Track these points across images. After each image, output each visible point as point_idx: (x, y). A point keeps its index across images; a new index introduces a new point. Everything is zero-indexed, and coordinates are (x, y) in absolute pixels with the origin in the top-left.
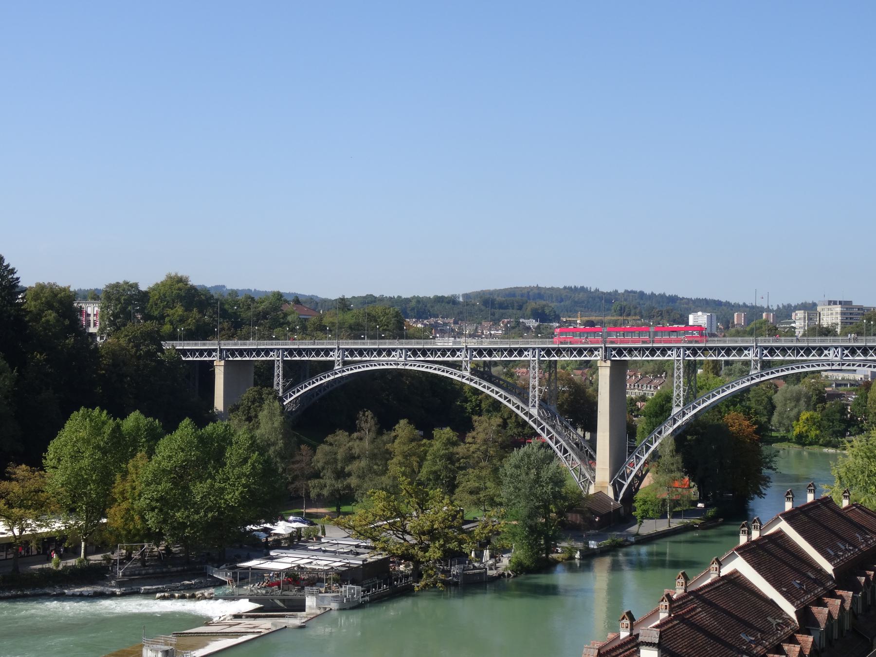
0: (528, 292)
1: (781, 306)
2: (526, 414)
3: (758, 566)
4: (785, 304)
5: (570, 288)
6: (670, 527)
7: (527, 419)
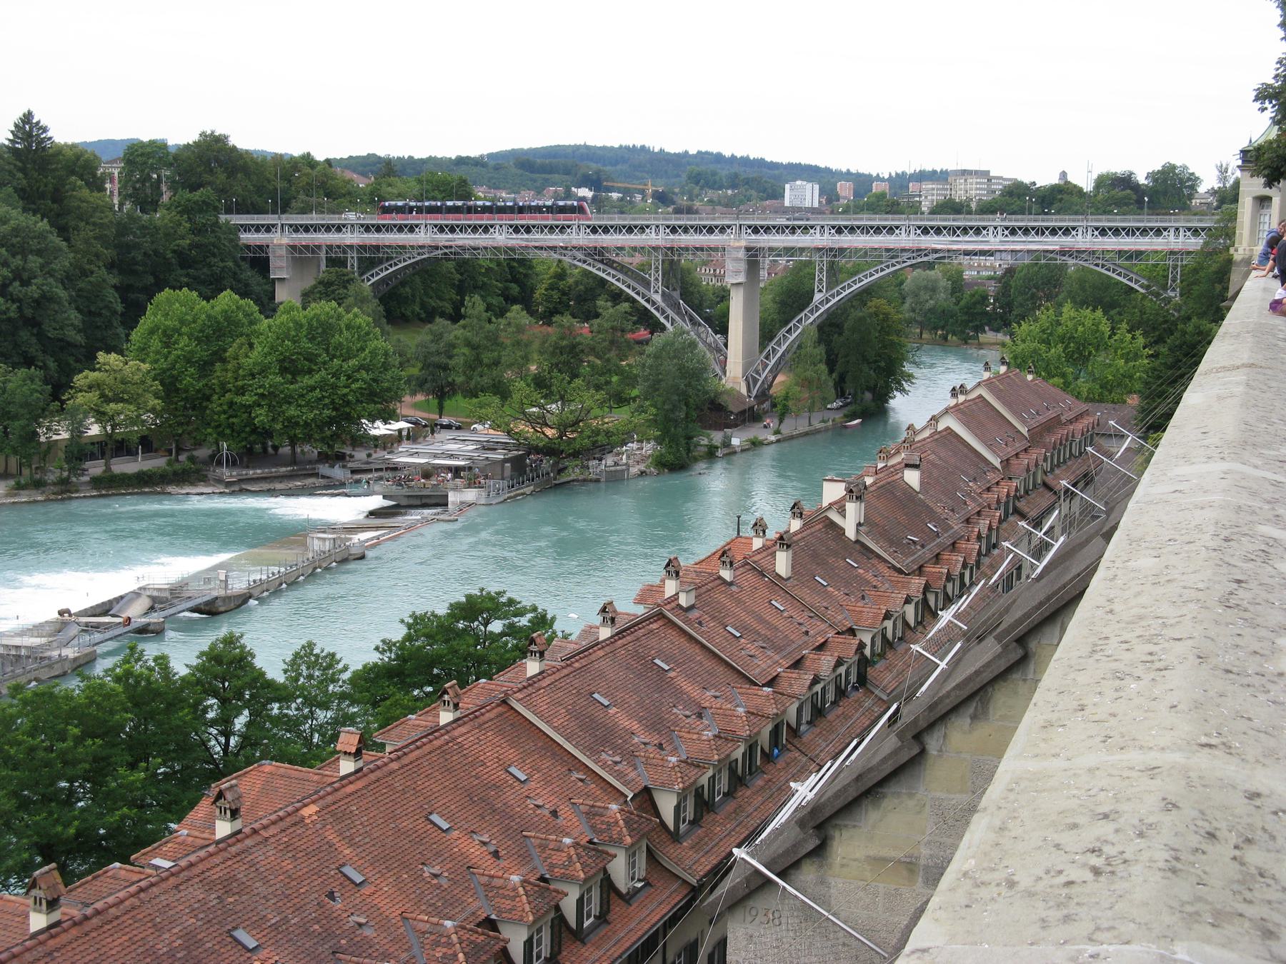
0: (574, 152)
1: (894, 174)
2: (648, 301)
3: (967, 424)
4: (900, 171)
5: (627, 148)
6: (810, 425)
7: (648, 306)
